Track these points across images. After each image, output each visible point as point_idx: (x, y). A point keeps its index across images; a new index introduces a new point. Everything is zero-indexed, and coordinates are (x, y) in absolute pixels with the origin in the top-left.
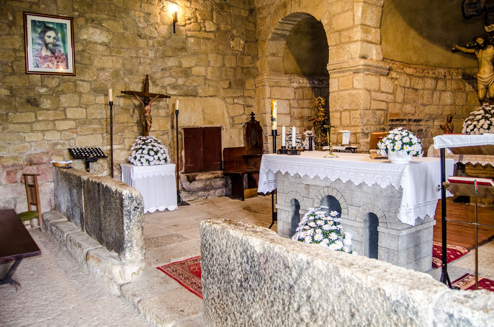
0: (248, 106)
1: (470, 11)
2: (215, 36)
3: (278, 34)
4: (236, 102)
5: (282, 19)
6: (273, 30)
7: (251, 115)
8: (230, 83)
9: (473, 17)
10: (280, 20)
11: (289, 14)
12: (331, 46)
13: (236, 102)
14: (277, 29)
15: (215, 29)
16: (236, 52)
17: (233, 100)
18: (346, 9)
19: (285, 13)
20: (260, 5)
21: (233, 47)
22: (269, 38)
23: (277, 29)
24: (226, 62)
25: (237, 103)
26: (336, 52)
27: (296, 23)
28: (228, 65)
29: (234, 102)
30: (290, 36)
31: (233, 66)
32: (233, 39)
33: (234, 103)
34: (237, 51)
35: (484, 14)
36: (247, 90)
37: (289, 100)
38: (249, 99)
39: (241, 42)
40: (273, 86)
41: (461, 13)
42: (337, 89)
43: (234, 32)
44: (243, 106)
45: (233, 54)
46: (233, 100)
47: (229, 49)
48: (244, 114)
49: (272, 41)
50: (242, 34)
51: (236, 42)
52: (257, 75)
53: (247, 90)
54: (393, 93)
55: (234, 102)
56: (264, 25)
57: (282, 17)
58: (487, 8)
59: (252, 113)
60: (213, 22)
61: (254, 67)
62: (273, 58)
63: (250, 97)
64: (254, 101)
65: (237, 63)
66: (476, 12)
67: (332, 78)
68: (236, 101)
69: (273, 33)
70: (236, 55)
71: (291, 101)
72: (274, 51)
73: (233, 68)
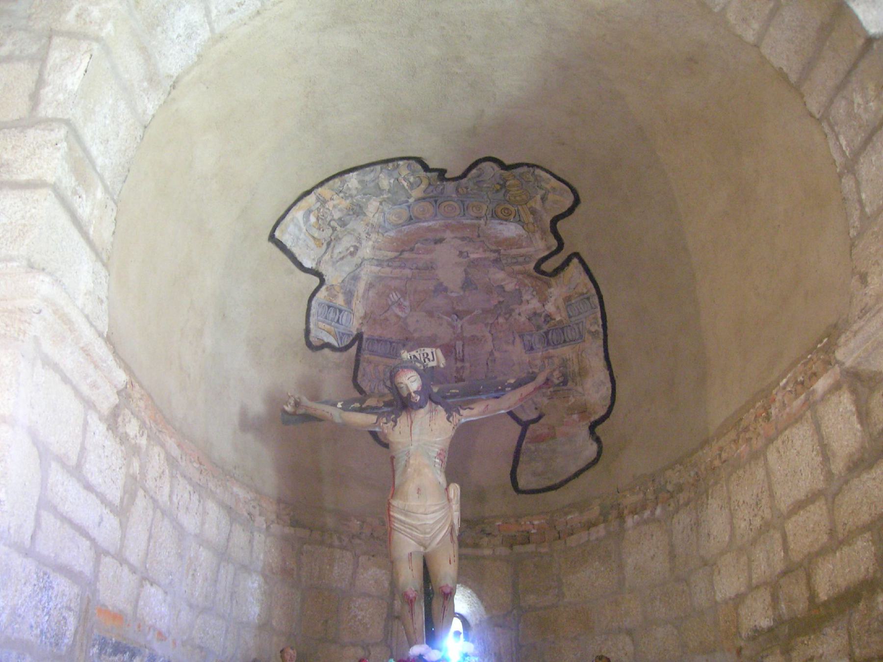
1: (322, 333)
9: (327, 351)
35: (354, 348)
41: (303, 326)
54: (122, 511)
58: (365, 336)
66: (335, 336)
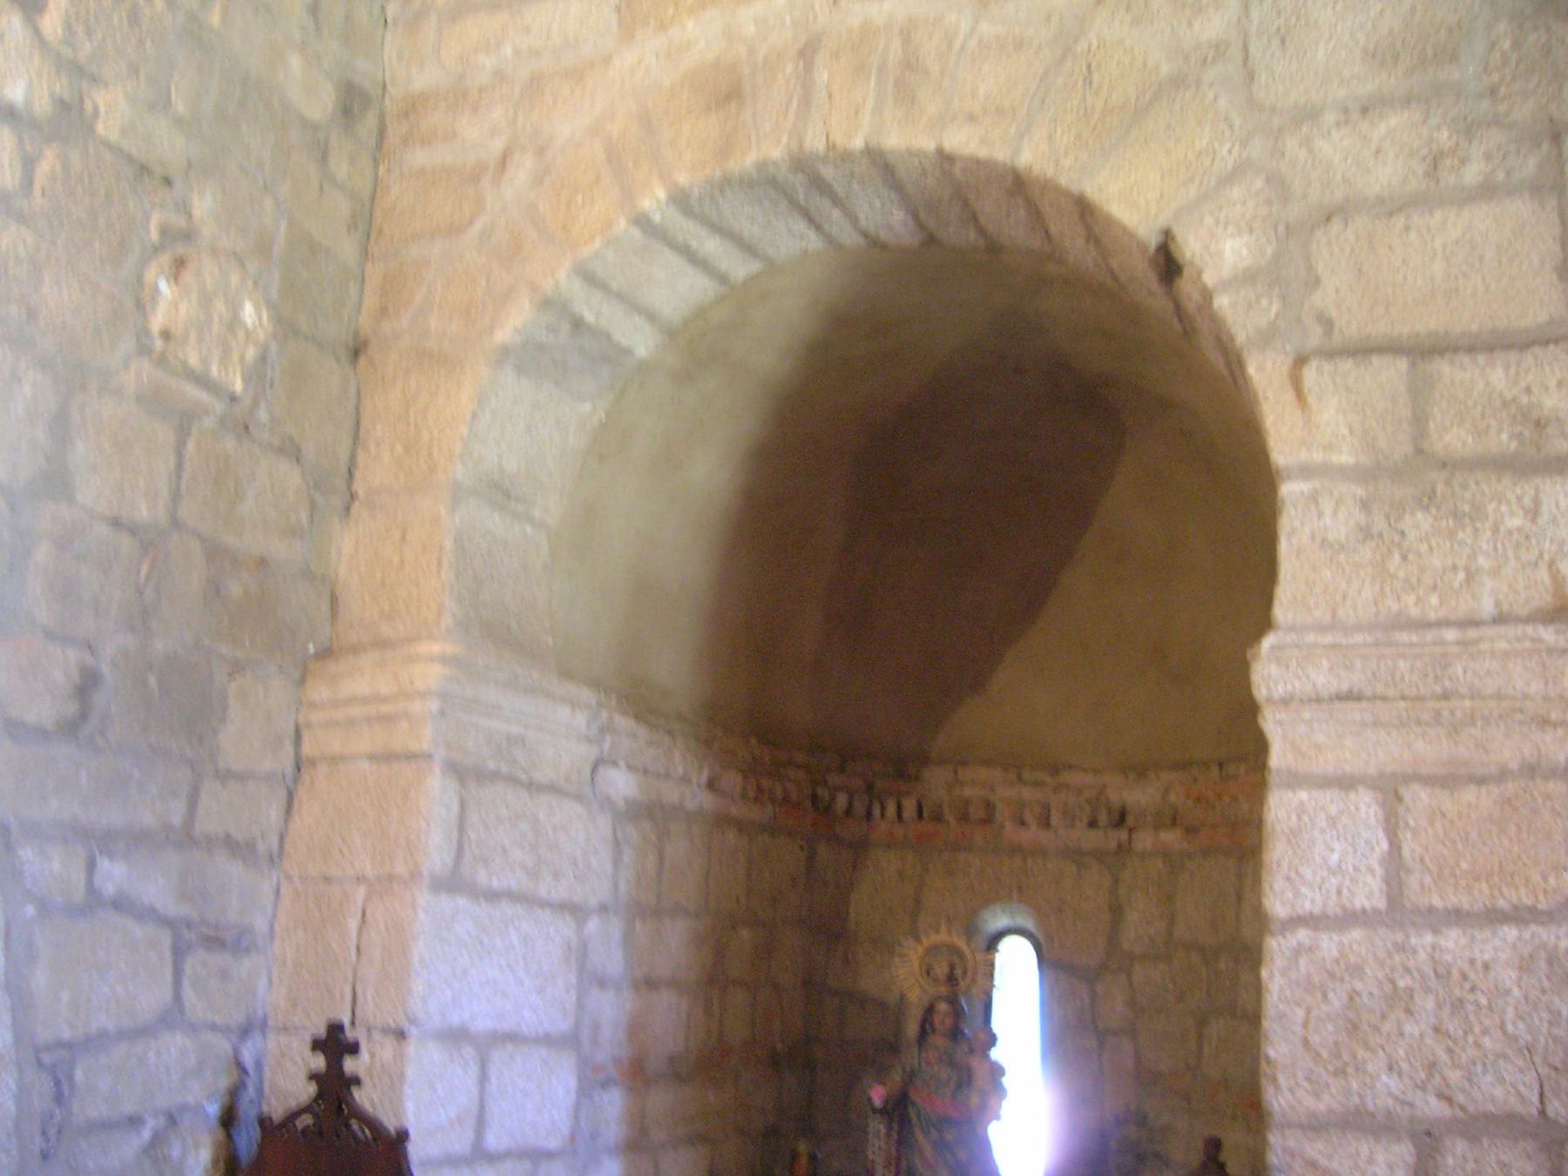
0: (215, 941)
2: (29, 164)
3: (578, 324)
4: (109, 889)
5: (681, 200)
6: (561, 278)
7: (317, 1045)
8: (87, 684)
10: (654, 200)
11: (776, 153)
12: (1307, 471)
13: (109, 889)
14: (590, 278)
15: (43, 106)
16: (192, 392)
17: (91, 867)
18: (1473, 173)
19: (725, 149)
20: (423, 79)
21: (166, 335)
22: (504, 334)
23: (590, 278)
24: (80, 451)
25: (120, 904)
26: (1366, 533)
27: (740, 268)
28: (93, 491)
29: (91, 889)
30: (644, 367)
31: (143, 512)
32: (180, 264)
33: (93, 902)
34: (202, 381)
36: (225, 776)
37: (575, 910)
38: (233, 870)
39: (248, 312)
40: (483, 776)
42: (1369, 893)
43: (203, 205)
44: (166, 938)
45: (154, 401)
46: (91, 867)
47: (127, 344)
48: (173, 1017)
49: (520, 370)
50: (263, 248)
51: (206, 300)
52: (326, 653)
53: (225, 776)
55: (91, 889)
56: (455, 229)
57: (682, 179)
59: (335, 1029)
60: (37, 32)
61: (308, 575)
62: (495, 522)
63: (240, 849)
64: (267, 888)
65: (176, 496)
67: (1296, 780)
68: (114, 874)
69: (546, 304)
70: (184, 423)
71: (593, 925)
72: (511, 465)
73: (134, 530)
